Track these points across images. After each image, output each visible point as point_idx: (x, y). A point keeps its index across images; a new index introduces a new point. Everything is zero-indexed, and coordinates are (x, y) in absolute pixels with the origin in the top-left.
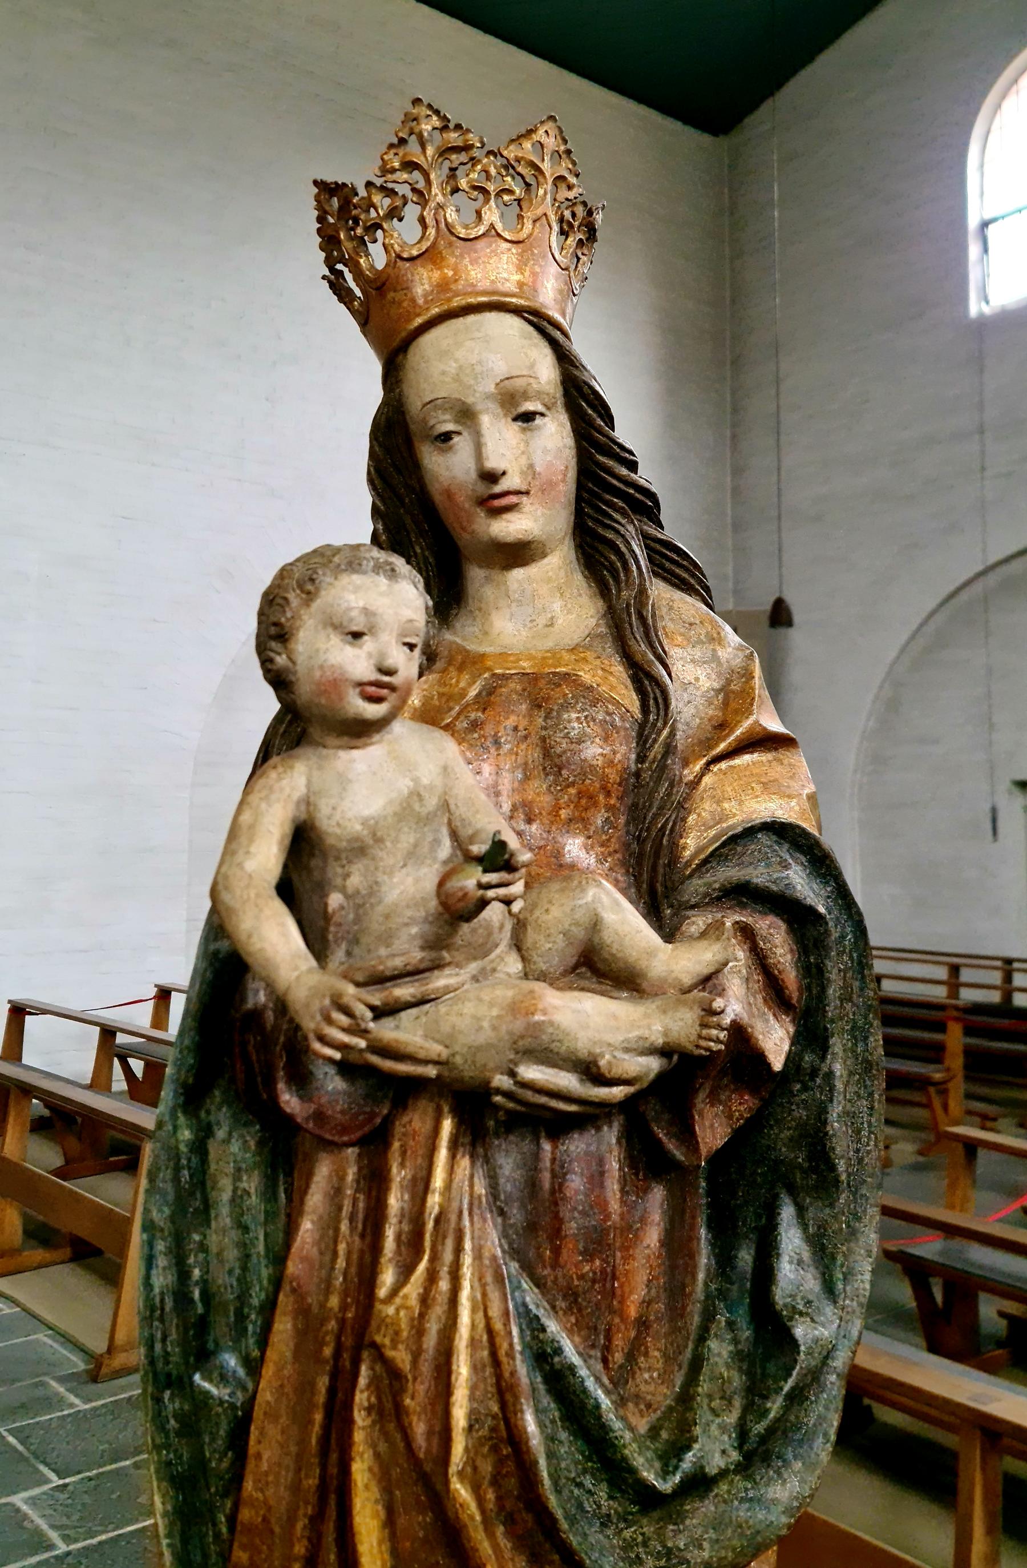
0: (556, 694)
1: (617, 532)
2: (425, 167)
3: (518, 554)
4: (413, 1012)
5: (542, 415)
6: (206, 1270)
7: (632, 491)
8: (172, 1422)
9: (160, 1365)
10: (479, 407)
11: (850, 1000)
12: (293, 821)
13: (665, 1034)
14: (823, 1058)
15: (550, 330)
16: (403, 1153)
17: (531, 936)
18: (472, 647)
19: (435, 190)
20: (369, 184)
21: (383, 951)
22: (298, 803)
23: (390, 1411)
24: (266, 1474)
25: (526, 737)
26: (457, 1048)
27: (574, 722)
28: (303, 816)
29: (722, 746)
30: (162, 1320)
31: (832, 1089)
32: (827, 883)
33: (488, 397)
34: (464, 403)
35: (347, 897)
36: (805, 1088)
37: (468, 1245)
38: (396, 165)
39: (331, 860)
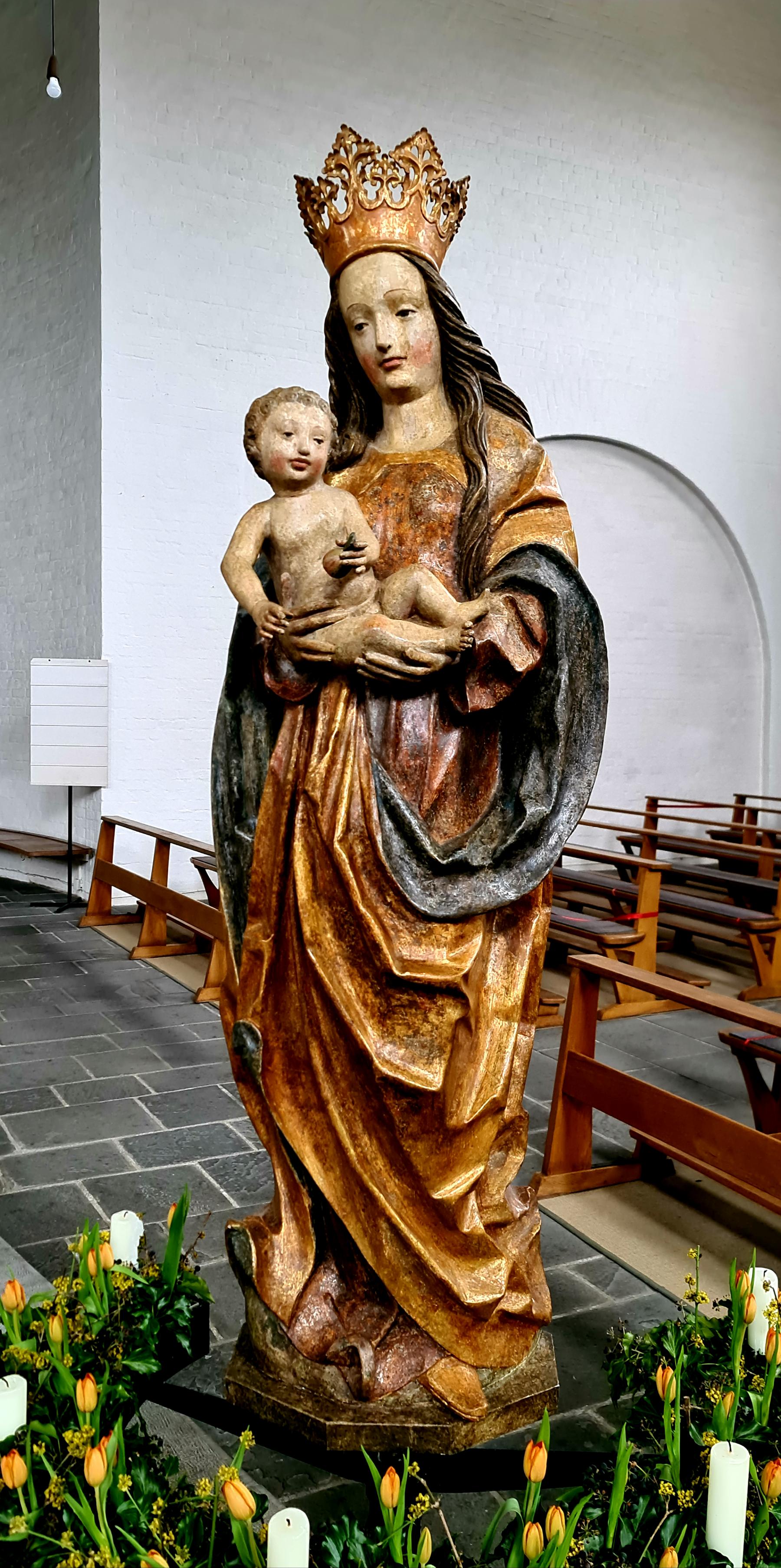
0: (421, 475)
1: (466, 381)
2: (348, 167)
3: (404, 395)
4: (321, 630)
5: (413, 311)
6: (240, 778)
7: (472, 355)
8: (229, 857)
9: (222, 829)
10: (375, 309)
11: (587, 649)
12: (263, 534)
13: (446, 642)
14: (555, 672)
15: (418, 261)
16: (325, 708)
17: (386, 597)
18: (382, 451)
19: (353, 181)
20: (319, 179)
21: (307, 600)
22: (266, 526)
23: (312, 823)
24: (262, 859)
25: (402, 499)
26: (339, 645)
27: (427, 490)
28: (269, 533)
29: (514, 504)
30: (222, 807)
31: (559, 687)
32: (570, 580)
33: (380, 302)
34: (367, 307)
35: (291, 574)
36: (547, 689)
37: (352, 748)
38: (333, 166)
39: (282, 554)
